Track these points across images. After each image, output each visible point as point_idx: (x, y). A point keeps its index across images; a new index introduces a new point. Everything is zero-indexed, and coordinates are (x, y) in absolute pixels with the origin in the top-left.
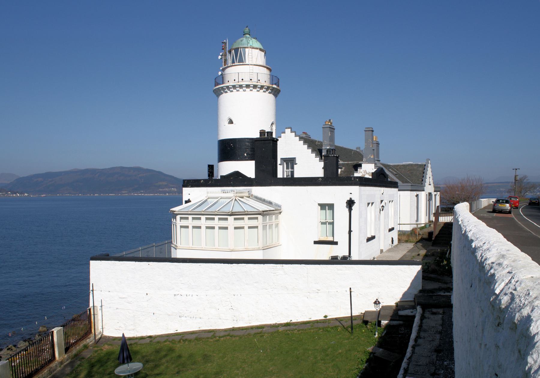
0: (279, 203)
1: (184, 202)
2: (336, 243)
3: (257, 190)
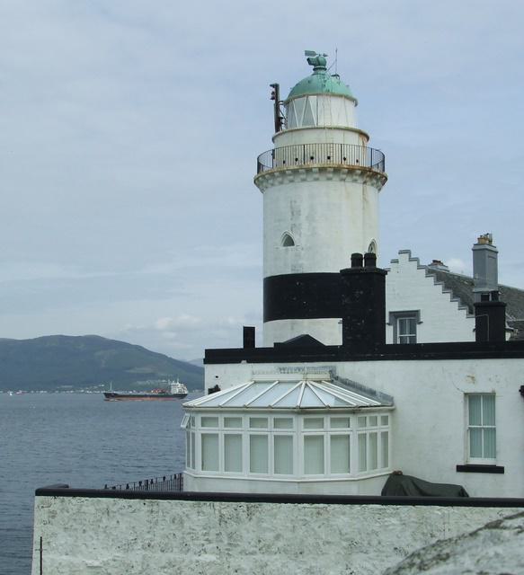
0: (388, 391)
1: (206, 391)
2: (500, 470)
3: (347, 369)
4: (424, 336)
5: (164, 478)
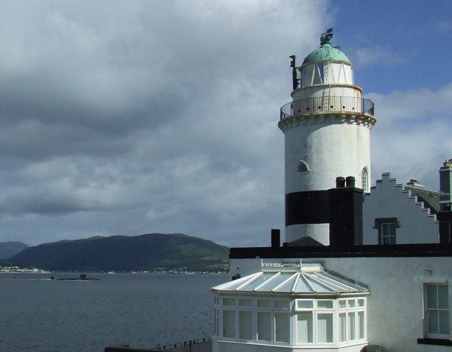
3: (333, 263)
4: (402, 238)
5: (204, 339)
